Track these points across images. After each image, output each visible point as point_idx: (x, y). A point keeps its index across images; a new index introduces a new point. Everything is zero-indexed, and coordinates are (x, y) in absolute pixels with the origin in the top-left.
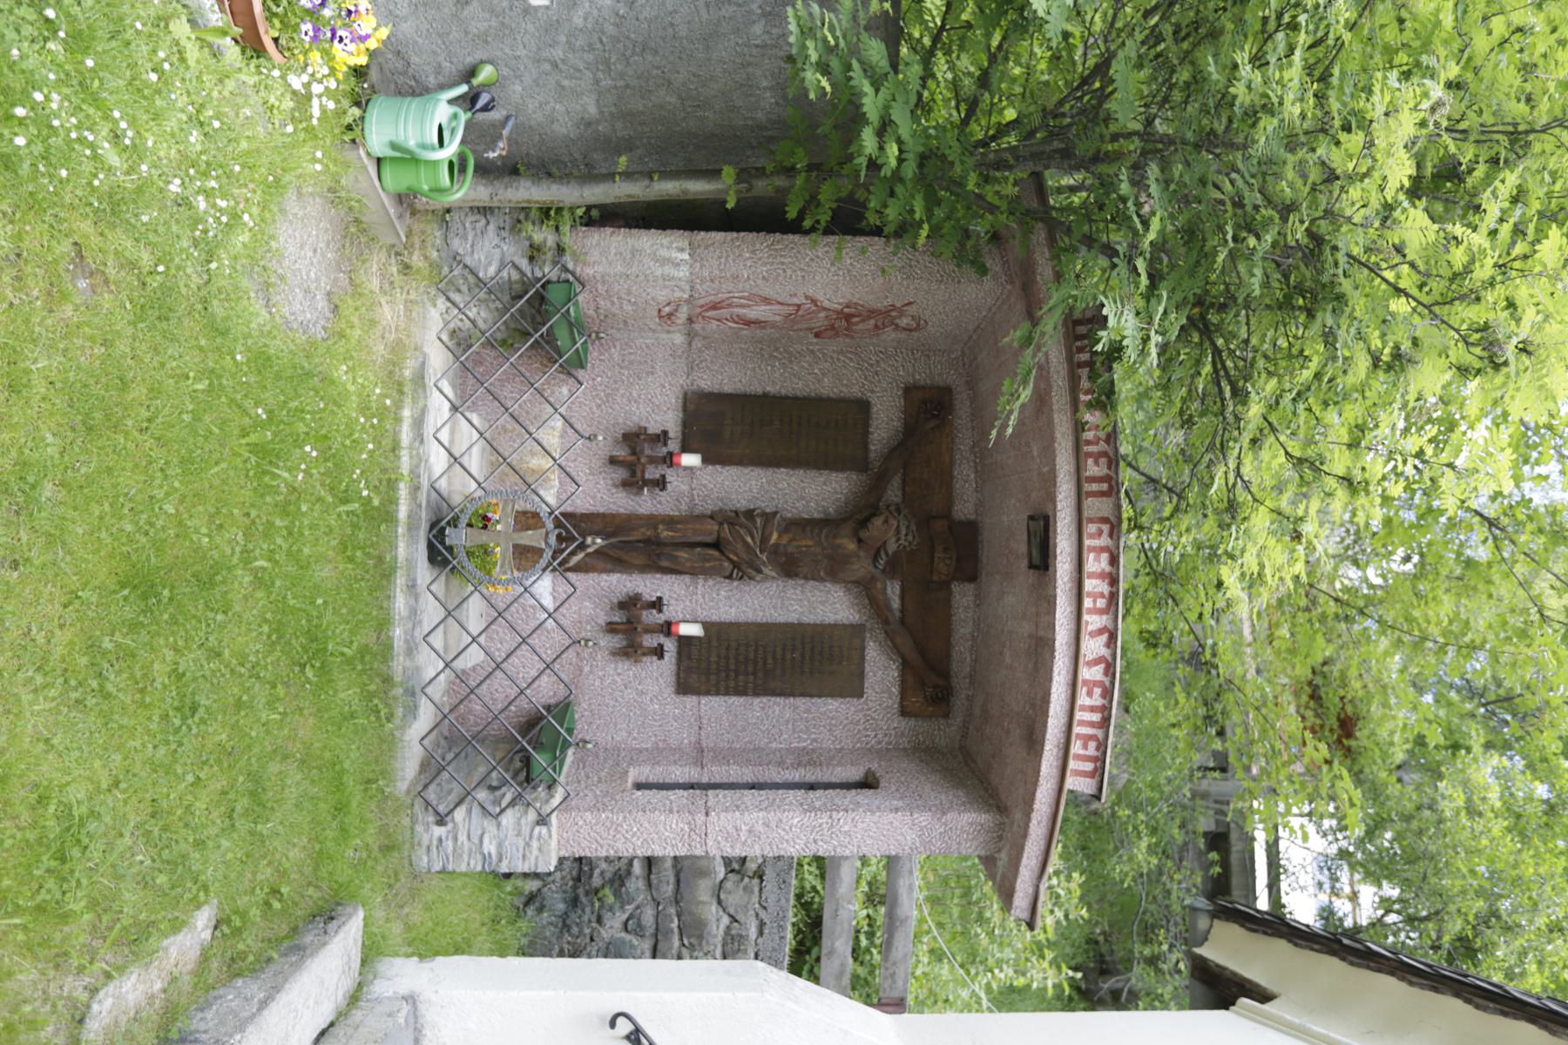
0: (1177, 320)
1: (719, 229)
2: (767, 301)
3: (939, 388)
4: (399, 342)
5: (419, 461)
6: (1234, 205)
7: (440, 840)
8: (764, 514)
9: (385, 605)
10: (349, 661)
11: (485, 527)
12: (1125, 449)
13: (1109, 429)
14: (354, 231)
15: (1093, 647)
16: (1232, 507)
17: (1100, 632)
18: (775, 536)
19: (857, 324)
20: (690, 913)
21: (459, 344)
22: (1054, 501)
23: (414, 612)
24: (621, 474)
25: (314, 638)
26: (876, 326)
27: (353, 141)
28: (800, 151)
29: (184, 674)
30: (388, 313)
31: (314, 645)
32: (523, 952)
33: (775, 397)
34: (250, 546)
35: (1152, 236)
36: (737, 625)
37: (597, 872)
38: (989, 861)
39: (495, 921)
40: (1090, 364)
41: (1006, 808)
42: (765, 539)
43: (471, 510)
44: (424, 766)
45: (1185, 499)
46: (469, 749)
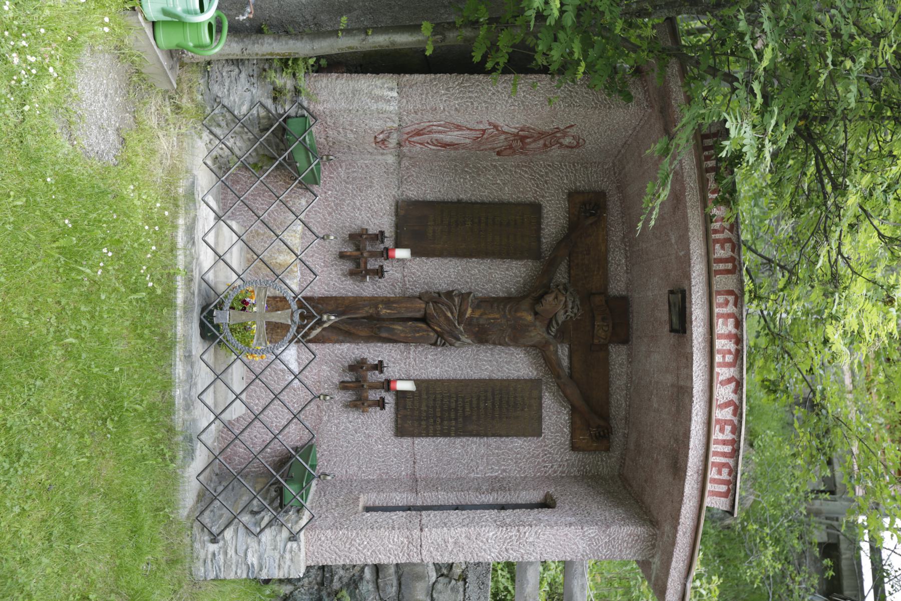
0: (787, 132)
2: (459, 127)
3: (595, 192)
4: (174, 166)
5: (192, 259)
6: (833, 35)
7: (214, 554)
9: (168, 371)
10: (141, 416)
11: (244, 309)
12: (745, 236)
13: (733, 220)
14: (136, 81)
15: (724, 393)
16: (835, 279)
17: (729, 381)
18: (469, 311)
21: (220, 168)
22: (689, 278)
23: (190, 376)
24: (348, 265)
26: (545, 145)
27: (133, 8)
28: (482, 8)
29: (11, 428)
30: (164, 144)
31: (113, 404)
33: (466, 203)
34: (62, 327)
35: (765, 63)
36: (441, 381)
37: (336, 578)
38: (645, 565)
40: (716, 169)
41: (657, 523)
42: (461, 314)
43: (233, 295)
44: (200, 497)
45: (797, 274)
46: (235, 483)
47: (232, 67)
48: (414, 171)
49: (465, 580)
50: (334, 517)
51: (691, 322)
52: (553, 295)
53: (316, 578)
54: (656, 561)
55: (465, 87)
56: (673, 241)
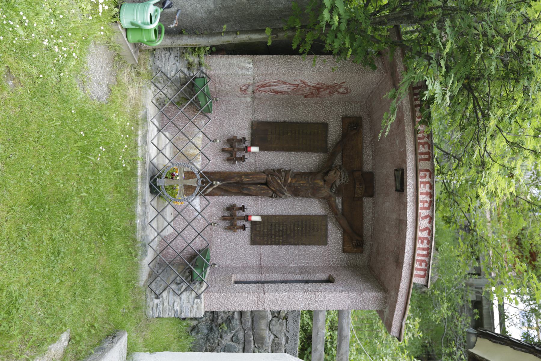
2: (285, 83)
5: (146, 152)
7: (157, 305)
8: (285, 171)
10: (120, 233)
15: (423, 223)
17: (426, 217)
19: (322, 91)
20: (258, 334)
25: (106, 224)
26: (330, 92)
36: (275, 216)
37: (220, 317)
39: (180, 337)
41: (388, 291)
42: (286, 181)
47: (166, 52)
48: (261, 106)
49: (286, 319)
51: (407, 186)
52: (334, 172)
55: (288, 62)
56: (397, 143)
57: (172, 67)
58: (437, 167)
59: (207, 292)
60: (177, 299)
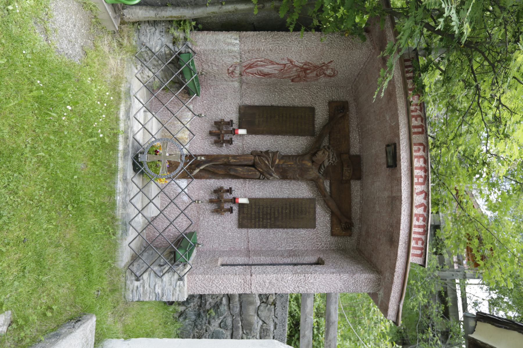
1: (251, 30)
2: (272, 63)
5: (128, 128)
7: (137, 287)
8: (272, 152)
10: (94, 208)
15: (419, 199)
17: (421, 193)
19: (308, 74)
20: (246, 320)
23: (126, 190)
25: (74, 193)
26: (317, 75)
32: (178, 336)
36: (263, 199)
37: (208, 303)
39: (166, 323)
41: (381, 272)
42: (273, 162)
47: (152, 27)
48: (248, 91)
49: (275, 305)
50: (204, 269)
51: (400, 160)
52: (322, 152)
53: (197, 303)
54: (381, 294)
55: (275, 38)
56: (388, 119)
57: (157, 41)
58: (431, 140)
59: (191, 274)
60: (158, 281)
